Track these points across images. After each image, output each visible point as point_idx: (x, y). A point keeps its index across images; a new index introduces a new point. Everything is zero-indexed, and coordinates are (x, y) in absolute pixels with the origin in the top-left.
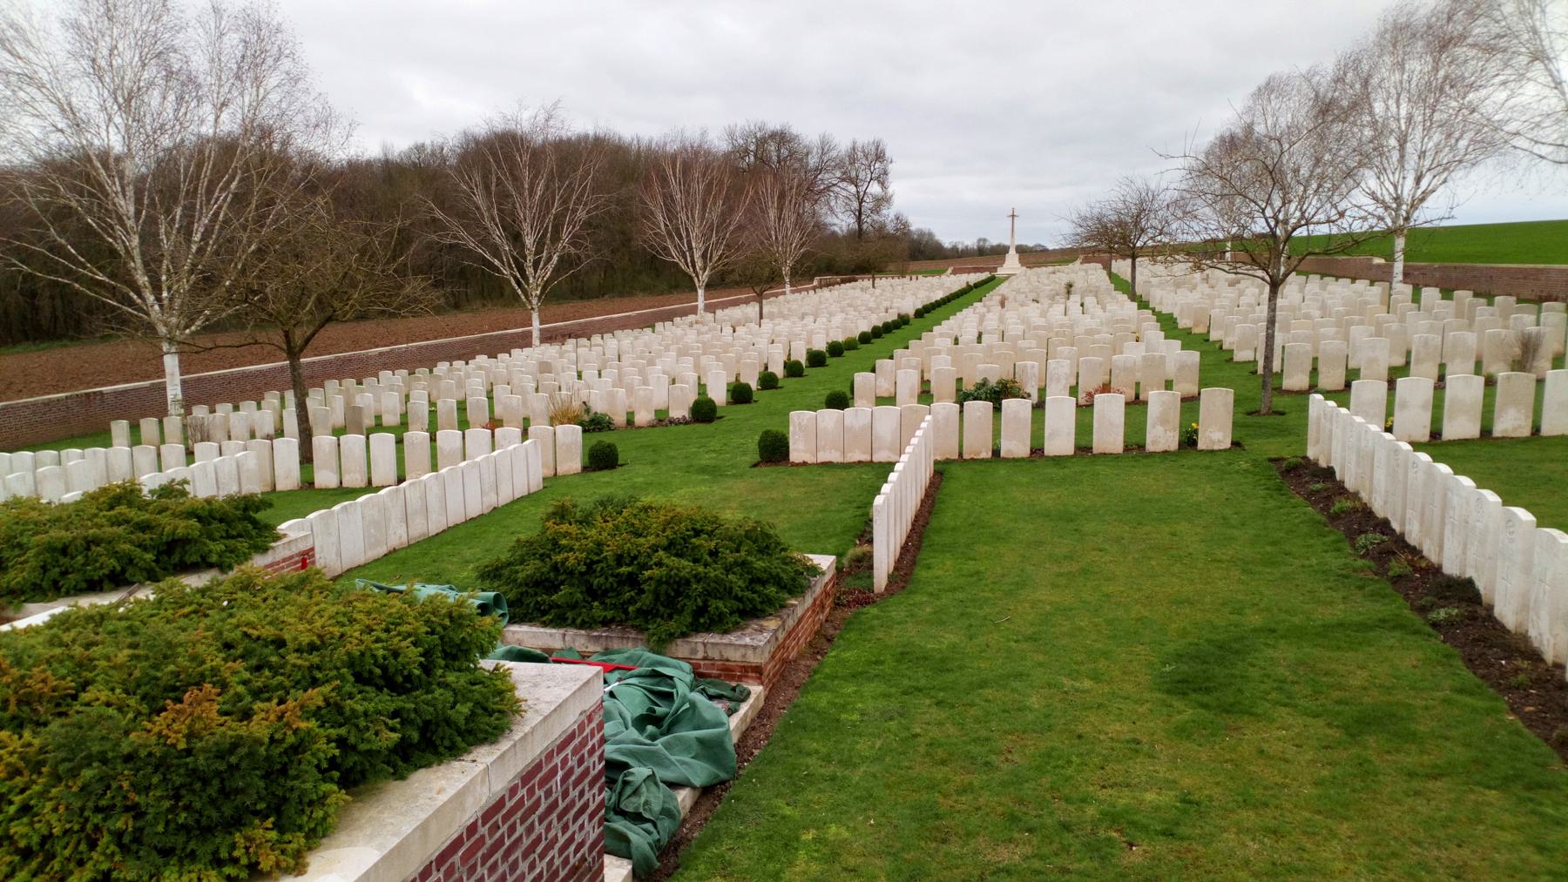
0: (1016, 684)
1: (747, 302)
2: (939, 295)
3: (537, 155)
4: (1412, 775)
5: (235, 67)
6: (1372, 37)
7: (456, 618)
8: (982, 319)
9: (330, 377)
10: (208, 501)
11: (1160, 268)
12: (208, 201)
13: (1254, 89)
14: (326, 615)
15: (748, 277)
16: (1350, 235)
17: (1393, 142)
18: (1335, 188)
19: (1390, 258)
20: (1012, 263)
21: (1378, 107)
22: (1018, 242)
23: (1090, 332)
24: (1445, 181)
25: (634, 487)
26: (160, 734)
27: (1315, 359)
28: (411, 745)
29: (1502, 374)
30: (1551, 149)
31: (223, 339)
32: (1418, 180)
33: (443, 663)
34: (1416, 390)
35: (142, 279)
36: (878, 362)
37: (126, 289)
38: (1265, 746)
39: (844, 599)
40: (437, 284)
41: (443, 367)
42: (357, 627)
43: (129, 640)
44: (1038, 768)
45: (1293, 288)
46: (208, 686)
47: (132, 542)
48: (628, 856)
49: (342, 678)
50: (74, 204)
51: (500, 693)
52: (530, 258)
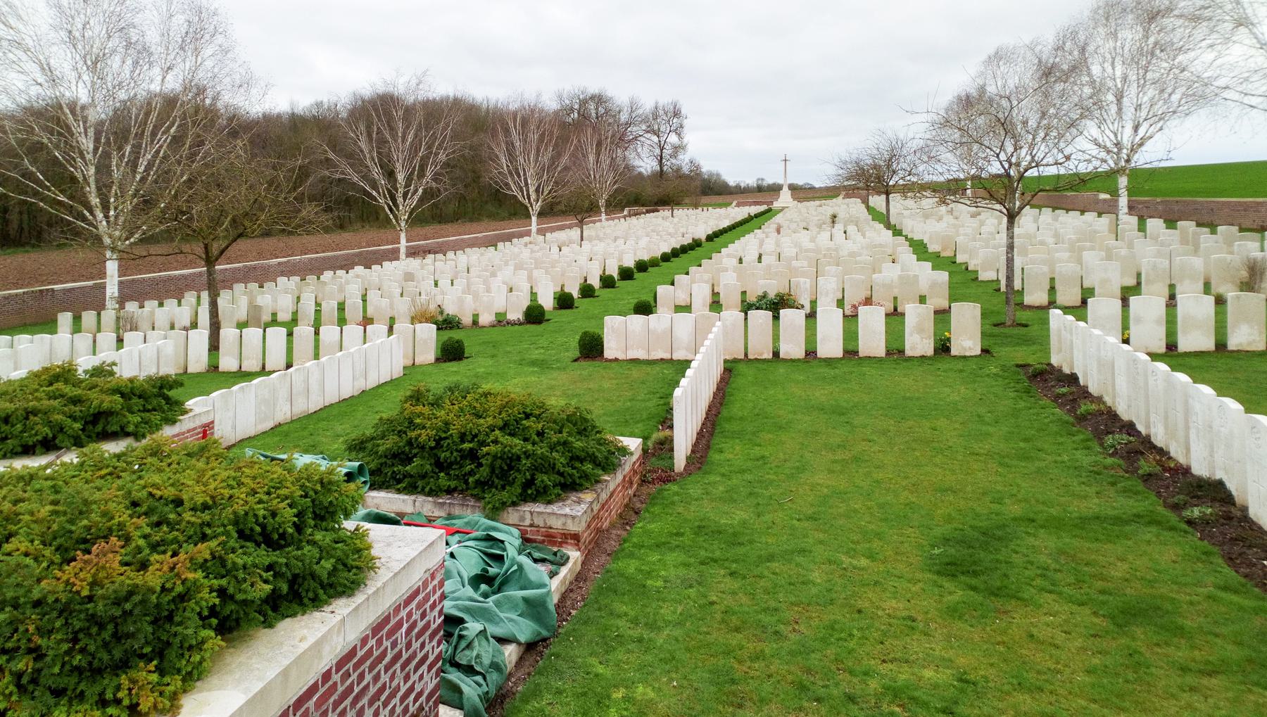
0: (799, 559)
1: (570, 227)
2: (726, 223)
3: (409, 111)
4: (1184, 670)
5: (180, 40)
6: (1087, 13)
7: (326, 484)
8: (761, 243)
9: (238, 281)
10: (131, 380)
11: (910, 203)
12: (152, 142)
13: (984, 57)
14: (219, 478)
15: (571, 207)
16: (1076, 174)
17: (1110, 97)
18: (1060, 136)
19: (1115, 193)
20: (785, 198)
21: (1096, 70)
22: (790, 182)
23: (852, 254)
24: (1161, 129)
25: (476, 376)
26: (67, 582)
27: (1052, 279)
28: (280, 596)
29: (1231, 294)
30: (1261, 99)
31: (154, 249)
32: (1136, 128)
33: (312, 523)
34: (1148, 307)
35: (95, 200)
36: (677, 277)
37: (81, 208)
38: (1035, 631)
39: (649, 477)
40: (327, 210)
41: (327, 275)
42: (244, 489)
43: (52, 498)
44: (823, 640)
45: (1028, 219)
46: (113, 539)
47: (64, 413)
48: (461, 708)
49: (227, 534)
50: (45, 141)
51: (359, 551)
52: (401, 190)
